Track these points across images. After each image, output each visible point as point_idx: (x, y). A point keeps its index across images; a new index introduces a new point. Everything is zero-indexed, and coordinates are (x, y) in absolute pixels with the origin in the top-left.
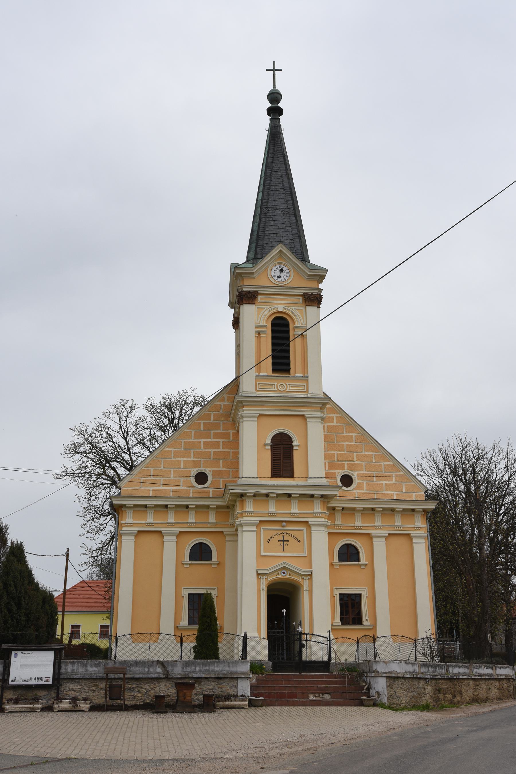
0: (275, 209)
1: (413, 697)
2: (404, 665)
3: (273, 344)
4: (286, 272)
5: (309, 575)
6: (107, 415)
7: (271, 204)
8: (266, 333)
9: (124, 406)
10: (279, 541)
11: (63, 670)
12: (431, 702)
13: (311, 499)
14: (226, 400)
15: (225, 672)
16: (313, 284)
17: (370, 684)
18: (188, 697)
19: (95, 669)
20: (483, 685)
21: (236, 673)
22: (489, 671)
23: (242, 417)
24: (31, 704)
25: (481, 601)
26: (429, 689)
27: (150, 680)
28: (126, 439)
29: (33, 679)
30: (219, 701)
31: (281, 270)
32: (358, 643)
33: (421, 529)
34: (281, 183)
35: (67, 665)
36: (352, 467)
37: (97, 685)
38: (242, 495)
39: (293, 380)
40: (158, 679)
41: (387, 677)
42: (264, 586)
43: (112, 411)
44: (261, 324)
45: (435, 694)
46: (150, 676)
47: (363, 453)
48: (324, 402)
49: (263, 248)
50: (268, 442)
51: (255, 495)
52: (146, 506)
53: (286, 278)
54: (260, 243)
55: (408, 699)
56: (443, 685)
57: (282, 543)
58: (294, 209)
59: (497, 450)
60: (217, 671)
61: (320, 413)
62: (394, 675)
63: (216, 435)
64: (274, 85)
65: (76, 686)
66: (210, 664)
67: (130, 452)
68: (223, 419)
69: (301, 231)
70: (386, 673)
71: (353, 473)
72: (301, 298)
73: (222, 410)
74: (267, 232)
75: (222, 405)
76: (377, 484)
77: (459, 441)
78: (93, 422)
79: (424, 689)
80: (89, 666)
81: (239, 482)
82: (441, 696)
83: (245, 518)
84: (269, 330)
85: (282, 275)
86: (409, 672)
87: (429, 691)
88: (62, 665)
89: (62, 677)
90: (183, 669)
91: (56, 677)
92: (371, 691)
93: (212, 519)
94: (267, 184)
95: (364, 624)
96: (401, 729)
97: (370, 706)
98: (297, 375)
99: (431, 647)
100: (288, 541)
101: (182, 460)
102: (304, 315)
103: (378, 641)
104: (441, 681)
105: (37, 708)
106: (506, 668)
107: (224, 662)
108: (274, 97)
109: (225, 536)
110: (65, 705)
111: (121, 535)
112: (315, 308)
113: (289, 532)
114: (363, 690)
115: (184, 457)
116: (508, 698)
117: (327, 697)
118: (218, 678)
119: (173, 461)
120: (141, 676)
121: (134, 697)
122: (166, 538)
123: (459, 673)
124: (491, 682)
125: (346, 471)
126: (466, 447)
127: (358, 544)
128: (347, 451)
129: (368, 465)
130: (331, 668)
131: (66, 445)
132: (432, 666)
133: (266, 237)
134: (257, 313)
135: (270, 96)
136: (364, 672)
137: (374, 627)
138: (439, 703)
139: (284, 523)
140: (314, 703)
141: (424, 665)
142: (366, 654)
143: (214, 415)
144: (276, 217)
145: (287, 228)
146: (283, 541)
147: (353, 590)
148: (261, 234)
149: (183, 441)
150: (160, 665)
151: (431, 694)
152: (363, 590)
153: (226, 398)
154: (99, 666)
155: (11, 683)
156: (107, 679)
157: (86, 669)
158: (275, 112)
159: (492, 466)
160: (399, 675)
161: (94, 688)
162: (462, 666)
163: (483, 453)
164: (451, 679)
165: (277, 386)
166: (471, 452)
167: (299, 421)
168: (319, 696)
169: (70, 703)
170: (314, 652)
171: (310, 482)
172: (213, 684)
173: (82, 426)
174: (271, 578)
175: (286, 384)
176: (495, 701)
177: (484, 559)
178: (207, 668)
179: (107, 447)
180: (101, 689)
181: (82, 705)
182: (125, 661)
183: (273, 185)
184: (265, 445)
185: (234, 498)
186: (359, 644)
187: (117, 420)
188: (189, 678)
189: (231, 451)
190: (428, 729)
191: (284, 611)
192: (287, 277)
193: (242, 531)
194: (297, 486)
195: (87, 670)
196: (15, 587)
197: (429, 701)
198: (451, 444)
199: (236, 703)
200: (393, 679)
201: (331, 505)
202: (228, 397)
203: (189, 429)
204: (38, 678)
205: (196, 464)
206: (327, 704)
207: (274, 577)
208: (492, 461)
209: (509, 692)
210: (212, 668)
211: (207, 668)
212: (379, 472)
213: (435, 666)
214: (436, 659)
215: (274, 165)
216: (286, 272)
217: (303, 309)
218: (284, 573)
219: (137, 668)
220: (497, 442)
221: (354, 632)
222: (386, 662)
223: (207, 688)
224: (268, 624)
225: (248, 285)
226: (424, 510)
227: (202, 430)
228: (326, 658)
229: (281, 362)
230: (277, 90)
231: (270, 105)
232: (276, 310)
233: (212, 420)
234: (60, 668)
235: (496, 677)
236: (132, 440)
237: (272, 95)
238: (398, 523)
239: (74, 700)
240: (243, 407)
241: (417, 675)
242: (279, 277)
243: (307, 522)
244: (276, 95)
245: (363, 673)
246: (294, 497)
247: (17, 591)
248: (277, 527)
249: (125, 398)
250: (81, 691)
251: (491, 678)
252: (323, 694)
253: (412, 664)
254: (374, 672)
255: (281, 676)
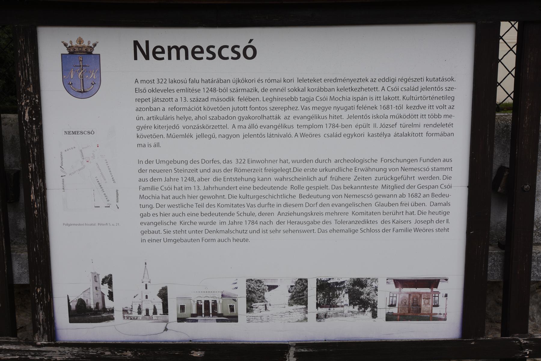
29: (279, 298)
155: (69, 330)
204: (328, 290)
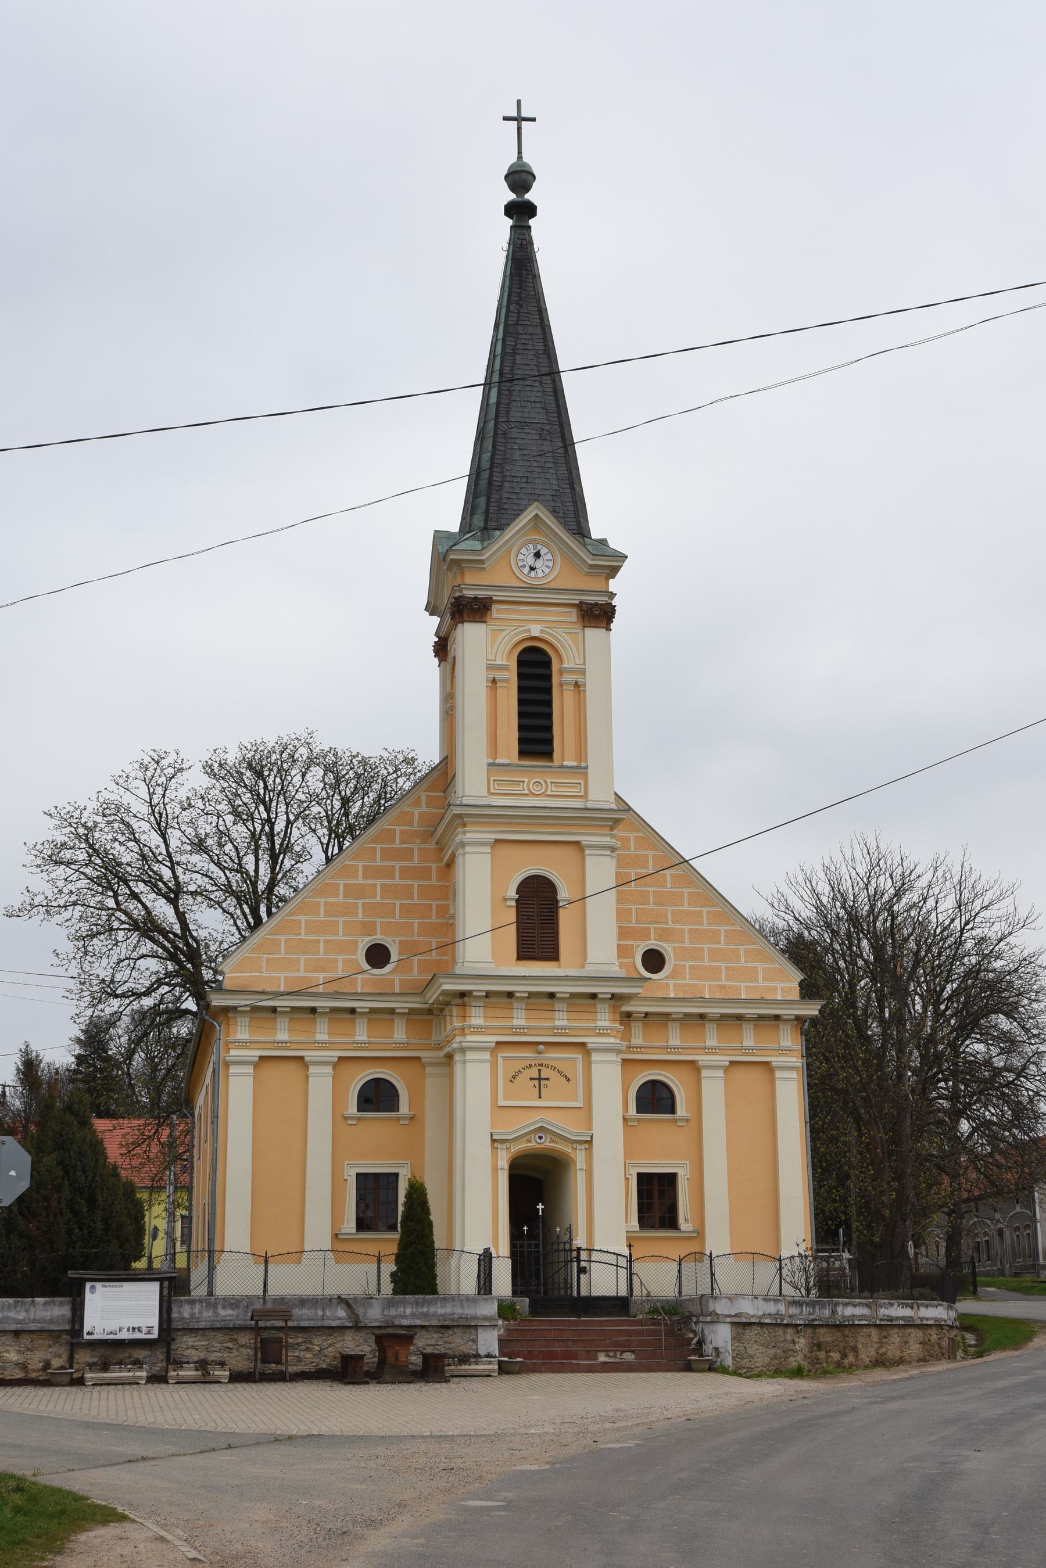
0: (523, 424)
1: (775, 1357)
2: (760, 1302)
3: (521, 702)
4: (546, 558)
5: (586, 1141)
6: (122, 781)
7: (515, 415)
8: (507, 681)
9: (158, 763)
10: (531, 1079)
11: (175, 1315)
12: (805, 1364)
13: (591, 1001)
14: (423, 804)
15: (456, 1316)
16: (595, 584)
17: (703, 1334)
18: (402, 1358)
19: (230, 1312)
20: (895, 1337)
21: (475, 1318)
22: (907, 1312)
23: (463, 844)
24: (129, 1371)
25: (899, 1177)
26: (802, 1343)
27: (327, 1331)
28: (163, 836)
29: (125, 1330)
30: (449, 1365)
31: (537, 555)
32: (680, 1265)
33: (792, 1053)
34: (535, 368)
35: (181, 1306)
36: (665, 935)
37: (235, 1340)
38: (463, 994)
39: (557, 772)
40: (342, 1329)
41: (732, 1323)
42: (504, 1163)
43: (133, 775)
44: (499, 662)
45: (812, 1352)
46: (327, 1323)
47: (686, 908)
48: (620, 817)
49: (500, 508)
50: (512, 892)
51: (488, 995)
52: (274, 1010)
53: (547, 571)
54: (495, 497)
55: (767, 1360)
56: (825, 1336)
57: (536, 1082)
58: (561, 426)
59: (940, 873)
60: (442, 1315)
61: (608, 839)
62: (744, 1320)
63: (405, 873)
64: (520, 152)
65: (199, 1340)
66: (429, 1303)
67: (171, 861)
68: (418, 841)
69: (574, 472)
70: (730, 1316)
71: (665, 945)
72: (574, 611)
73: (416, 824)
74: (507, 473)
75: (416, 812)
76: (711, 967)
77: (865, 851)
78: (94, 797)
79: (794, 1343)
80: (220, 1307)
81: (458, 970)
82: (822, 1355)
83: (469, 1038)
84: (511, 676)
85: (539, 564)
86: (770, 1314)
87: (802, 1346)
88: (173, 1306)
89: (174, 1325)
90: (383, 1310)
91: (165, 1326)
92: (705, 1347)
93: (400, 1033)
94: (507, 370)
95: (682, 1228)
96: (765, 1403)
97: (704, 1371)
98: (566, 763)
99: (806, 1271)
100: (548, 1079)
101: (341, 920)
102: (581, 645)
103: (716, 1261)
104: (822, 1331)
105: (141, 1378)
106: (937, 1306)
107: (453, 1299)
108: (520, 178)
109: (424, 1066)
110: (188, 1373)
111: (227, 1065)
112: (600, 632)
113: (550, 1063)
114: (690, 1345)
115: (343, 915)
116: (938, 1359)
117: (629, 1357)
118: (443, 1327)
119: (323, 922)
120: (312, 1323)
121: (299, 1360)
122: (312, 1070)
123: (854, 1315)
124: (909, 1331)
125: (652, 943)
126: (878, 864)
127: (676, 1085)
128: (655, 904)
129: (695, 930)
130: (633, 1309)
131: (30, 844)
132: (807, 1304)
133: (507, 485)
134: (489, 639)
135: (511, 177)
136: (691, 1315)
137: (699, 1234)
138: (818, 1366)
139: (541, 1047)
140: (606, 1368)
141: (794, 1303)
142: (695, 1285)
143: (402, 832)
144: (525, 441)
145: (548, 465)
146: (540, 1079)
147: (663, 1165)
148: (497, 478)
149: (341, 882)
150: (343, 1305)
151: (805, 1351)
152: (682, 1166)
153: (423, 798)
154: (238, 1307)
155: (86, 1337)
156: (256, 1330)
157: (214, 1312)
158: (521, 212)
159: (931, 903)
160: (753, 1320)
161: (230, 1345)
162: (859, 1304)
163: (912, 878)
164: (838, 1327)
165: (528, 786)
166: (888, 875)
167: (569, 852)
168: (615, 1357)
169: (197, 1370)
170: (603, 1281)
171: (590, 970)
172: (436, 1336)
173: (72, 809)
174: (517, 1148)
175: (546, 782)
176: (915, 1364)
177: (907, 1097)
178: (425, 1310)
179: (126, 855)
180: (242, 1346)
181: (216, 1373)
182: (283, 1299)
183: (519, 372)
184: (505, 899)
185: (447, 999)
186: (683, 1267)
187: (143, 792)
188: (394, 1326)
189: (434, 903)
190: (806, 1401)
191: (540, 1207)
192: (549, 570)
193: (464, 1062)
194: (567, 978)
195: (216, 1314)
196: (84, 1171)
197: (802, 1362)
198: (848, 856)
199: (477, 1367)
200: (741, 1326)
201: (626, 1008)
202: (427, 796)
203: (353, 859)
204: (134, 1329)
205: (368, 928)
206: (629, 1368)
207: (522, 1146)
208: (931, 893)
209: (941, 1348)
210: (432, 1309)
211: (425, 1310)
212: (714, 944)
213: (812, 1304)
214: (813, 1292)
215: (520, 330)
216: (546, 558)
217: (577, 634)
218: (540, 1138)
219: (304, 1311)
220: (942, 857)
221: (660, 1241)
222: (731, 1298)
223: (424, 1342)
224: (511, 1230)
225: (473, 584)
226: (798, 1018)
227: (378, 862)
228: (623, 1292)
229: (536, 737)
230: (525, 164)
231: (512, 196)
232: (526, 635)
233: (397, 841)
234: (169, 1311)
235: (918, 1322)
236: (175, 838)
237: (517, 176)
238: (749, 1042)
239: (203, 1365)
240: (465, 825)
241: (782, 1320)
242: (532, 569)
243: (583, 1045)
244: (524, 175)
245: (691, 1315)
246: (559, 998)
247: (87, 1177)
248: (528, 1054)
249: (161, 747)
250: (207, 1349)
251: (908, 1324)
252: (622, 1352)
253: (774, 1300)
254: (710, 1314)
255: (545, 1323)
